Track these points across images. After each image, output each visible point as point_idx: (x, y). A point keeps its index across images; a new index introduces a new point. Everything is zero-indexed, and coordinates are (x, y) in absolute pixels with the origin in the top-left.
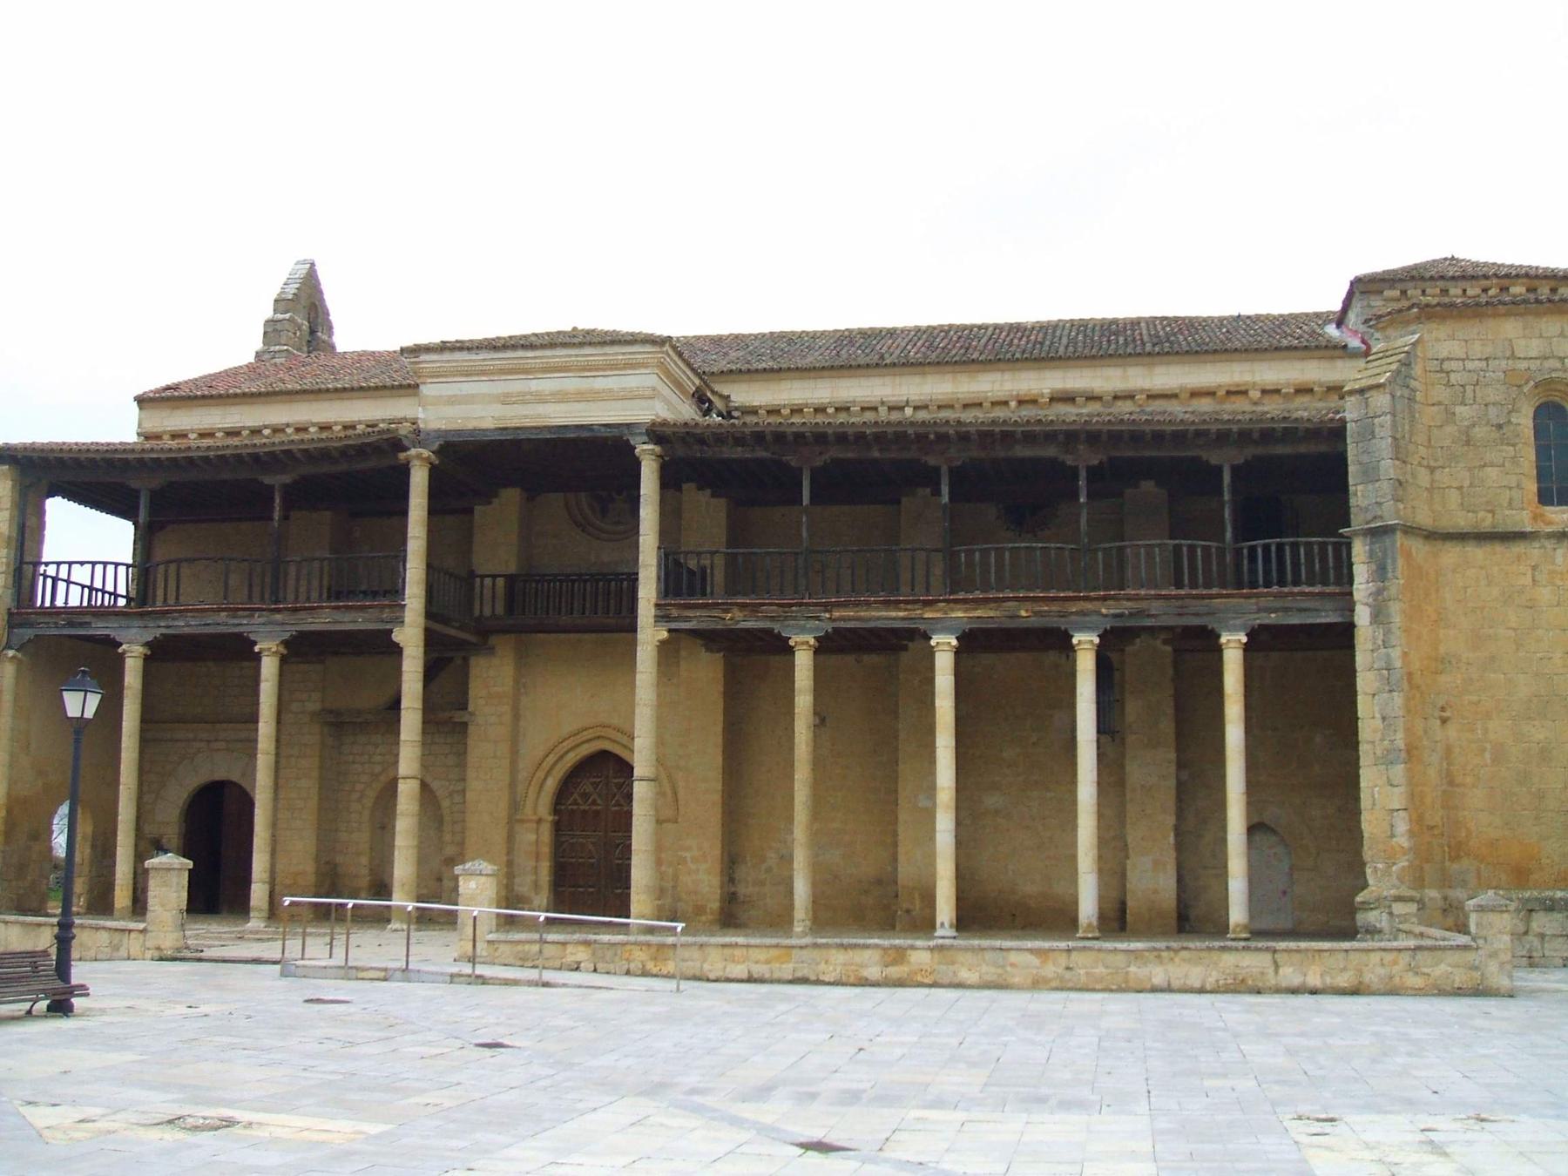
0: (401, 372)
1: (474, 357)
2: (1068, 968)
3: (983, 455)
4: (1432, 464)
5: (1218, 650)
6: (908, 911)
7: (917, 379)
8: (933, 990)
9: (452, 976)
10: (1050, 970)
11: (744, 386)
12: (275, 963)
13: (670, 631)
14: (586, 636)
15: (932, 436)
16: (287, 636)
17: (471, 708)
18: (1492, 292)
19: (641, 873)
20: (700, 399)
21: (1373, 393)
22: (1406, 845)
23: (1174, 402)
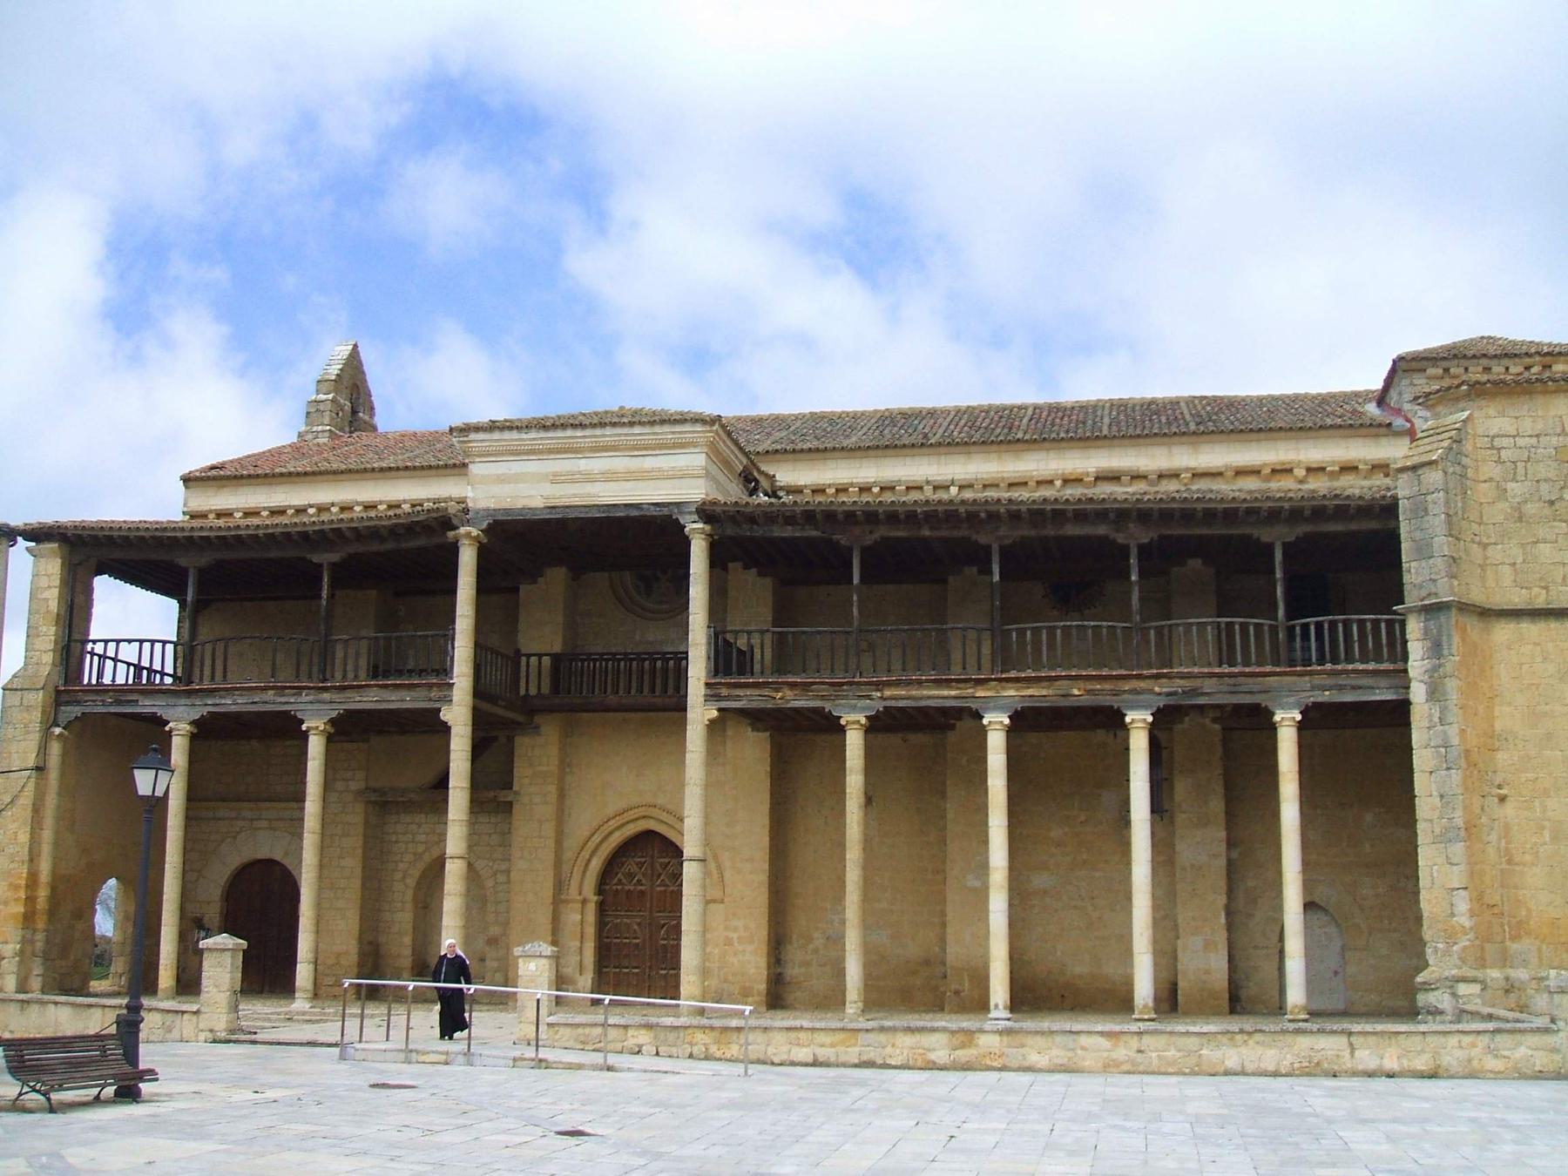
0: (447, 452)
1: (524, 436)
2: (1140, 1051)
3: (1033, 533)
4: (1485, 540)
5: (1272, 728)
6: (957, 993)
7: (962, 458)
8: (1003, 1074)
9: (515, 1060)
10: (1122, 1052)
11: (789, 466)
12: (336, 1045)
13: (719, 710)
14: (633, 715)
15: (983, 515)
16: (334, 714)
17: (516, 788)
18: (1534, 370)
19: (689, 955)
20: (749, 480)
21: (1425, 469)
22: (1467, 924)
23: (1219, 479)
